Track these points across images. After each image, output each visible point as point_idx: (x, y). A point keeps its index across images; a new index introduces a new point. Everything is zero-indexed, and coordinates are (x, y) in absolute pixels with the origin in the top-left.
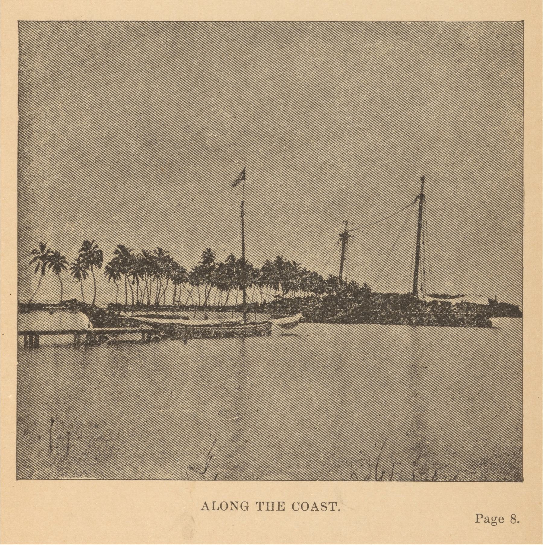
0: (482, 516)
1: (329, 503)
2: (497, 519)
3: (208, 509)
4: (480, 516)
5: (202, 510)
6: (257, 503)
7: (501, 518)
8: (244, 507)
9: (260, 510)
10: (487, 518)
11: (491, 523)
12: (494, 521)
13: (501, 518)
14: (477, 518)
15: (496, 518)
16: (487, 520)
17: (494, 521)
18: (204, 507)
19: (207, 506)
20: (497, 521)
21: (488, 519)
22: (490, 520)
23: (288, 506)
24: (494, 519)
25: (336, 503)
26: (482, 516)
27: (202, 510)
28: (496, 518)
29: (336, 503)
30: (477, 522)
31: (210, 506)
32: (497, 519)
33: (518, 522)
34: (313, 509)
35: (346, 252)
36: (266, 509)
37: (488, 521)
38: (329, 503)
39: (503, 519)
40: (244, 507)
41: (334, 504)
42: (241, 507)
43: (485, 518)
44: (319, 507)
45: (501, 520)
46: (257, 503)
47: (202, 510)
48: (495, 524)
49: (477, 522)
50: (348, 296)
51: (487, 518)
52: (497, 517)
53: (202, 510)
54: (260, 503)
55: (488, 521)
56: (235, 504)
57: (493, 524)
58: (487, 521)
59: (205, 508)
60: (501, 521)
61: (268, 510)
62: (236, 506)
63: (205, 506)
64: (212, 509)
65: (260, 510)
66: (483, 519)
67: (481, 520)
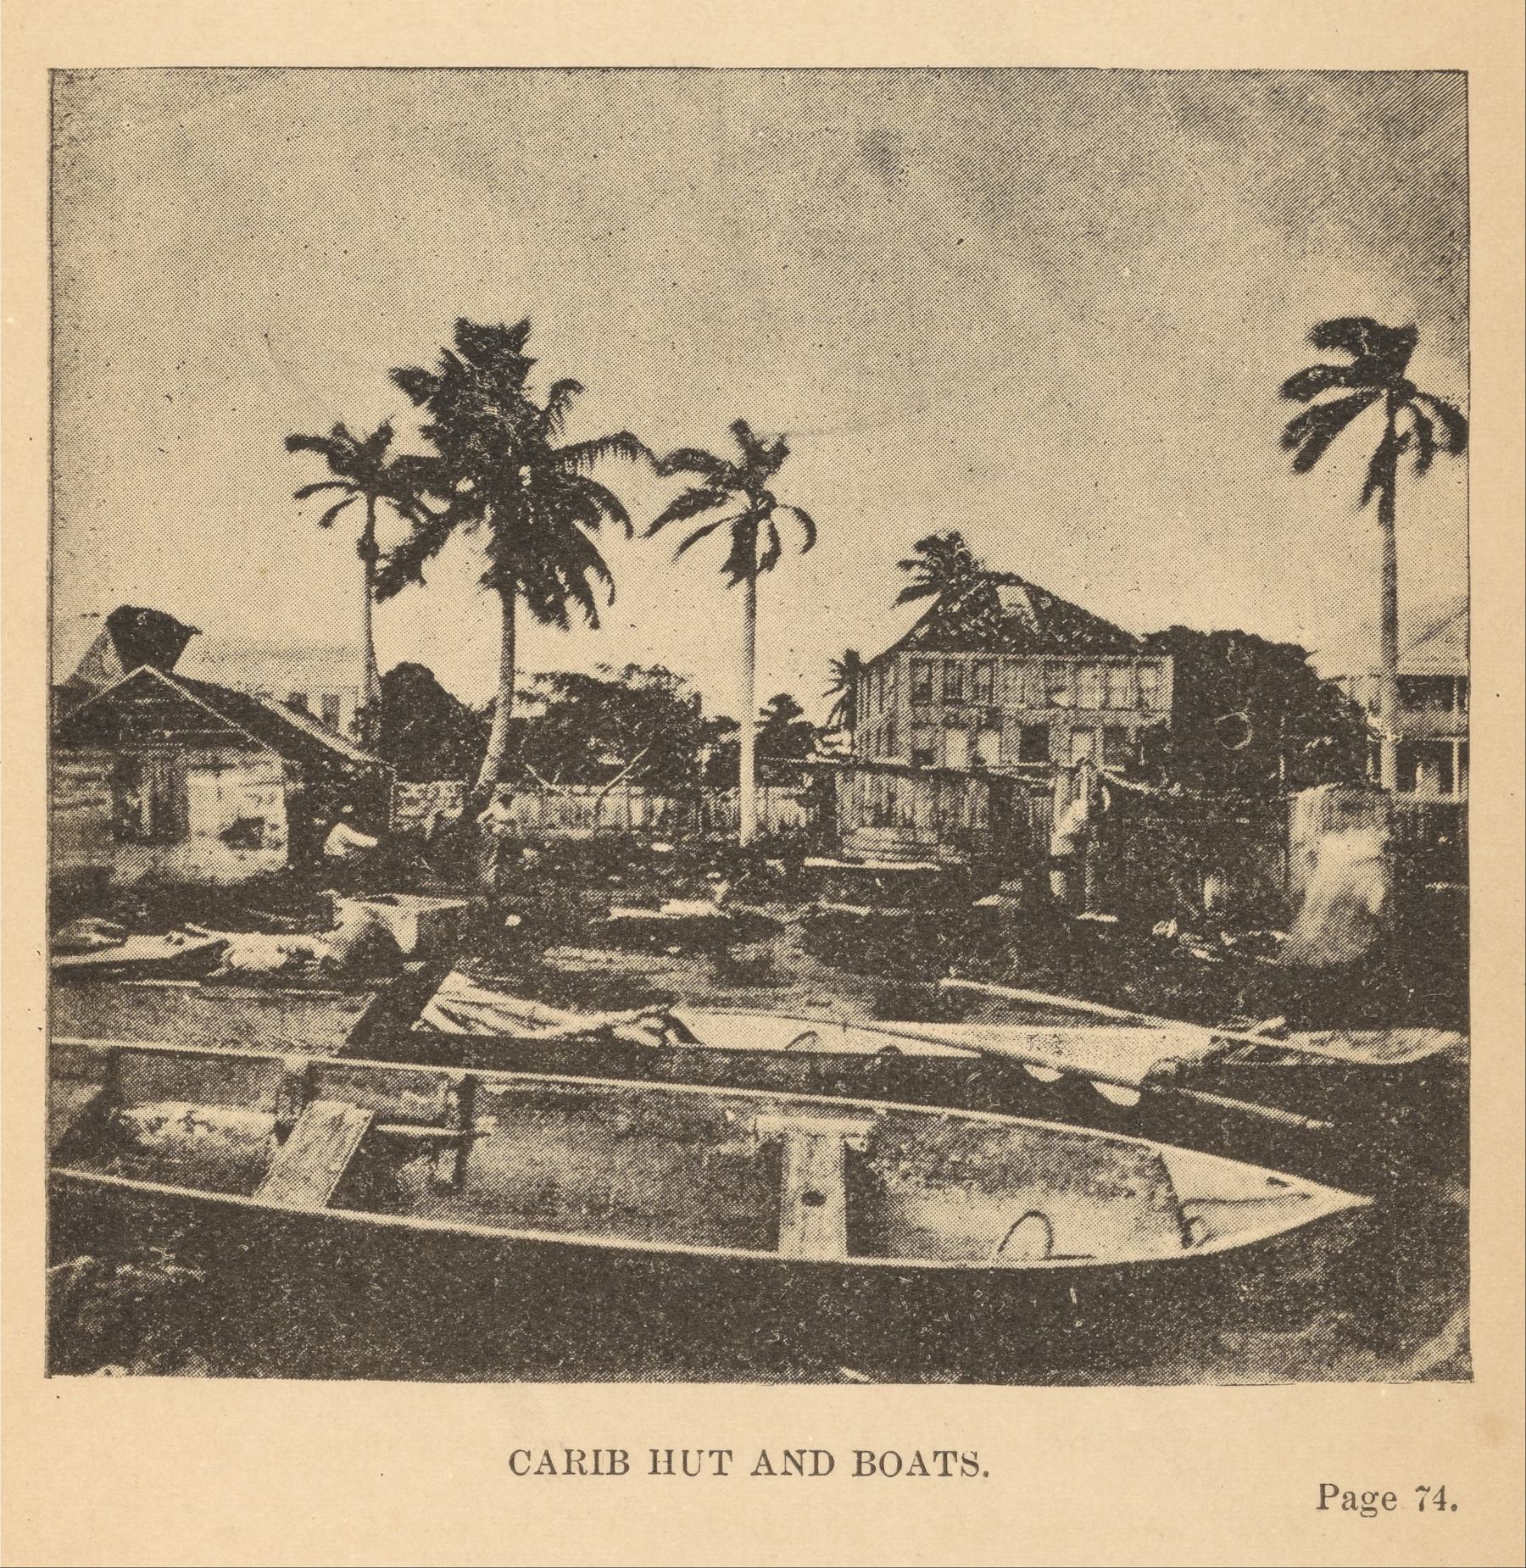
0: (1337, 1491)
1: (711, 1453)
2: (1379, 1499)
3: (771, 1472)
4: (1329, 1491)
5: (755, 1473)
6: (936, 1454)
7: (1389, 1497)
8: (820, 1462)
9: (720, 1472)
10: (1350, 1496)
11: (1360, 1509)
12: (1370, 1504)
13: (1389, 1497)
14: (1323, 1497)
15: (1374, 1496)
16: (1350, 1502)
17: (1370, 1504)
18: (759, 1465)
19: (550, 1463)
20: (1378, 1504)
21: (1353, 1499)
22: (1359, 1503)
23: (640, 1462)
24: (1368, 1498)
25: (730, 1453)
26: (1337, 1491)
27: (753, 1474)
28: (1374, 1496)
29: (730, 1453)
30: (1323, 1507)
31: (560, 1463)
32: (1379, 1499)
33: (1454, 1507)
34: (760, 1470)
35: (63, 395)
36: (941, 1472)
37: (1353, 1506)
38: (711, 1453)
39: (1394, 1499)
40: (820, 1462)
41: (725, 1455)
42: (882, 1468)
43: (1345, 1497)
44: (778, 1464)
45: (1389, 1500)
46: (936, 1454)
47: (755, 1473)
48: (1372, 1513)
49: (1323, 1507)
50: (1277, 777)
51: (1350, 1496)
52: (1377, 1494)
53: (753, 1474)
54: (945, 1454)
55: (1353, 1506)
56: (797, 1457)
57: (1366, 1513)
58: (1348, 1505)
59: (547, 1469)
60: (1390, 1505)
61: (655, 1471)
62: (788, 1459)
63: (763, 1462)
64: (812, 1471)
65: (720, 1472)
66: (1339, 1499)
67: (1334, 1503)
